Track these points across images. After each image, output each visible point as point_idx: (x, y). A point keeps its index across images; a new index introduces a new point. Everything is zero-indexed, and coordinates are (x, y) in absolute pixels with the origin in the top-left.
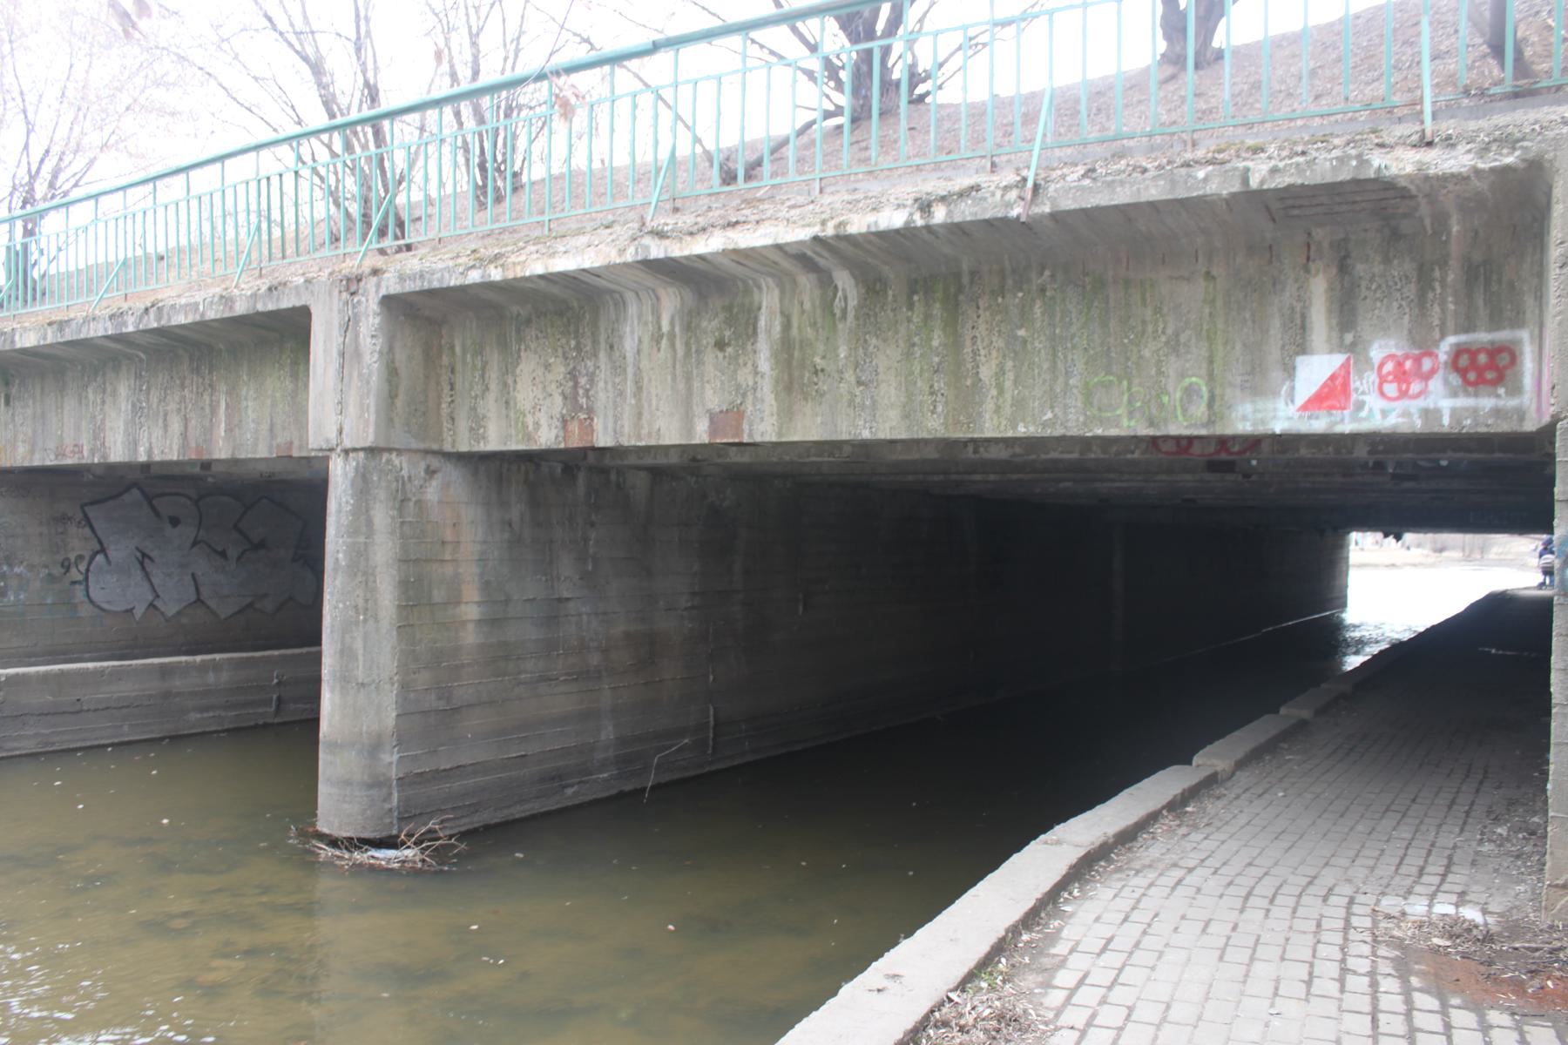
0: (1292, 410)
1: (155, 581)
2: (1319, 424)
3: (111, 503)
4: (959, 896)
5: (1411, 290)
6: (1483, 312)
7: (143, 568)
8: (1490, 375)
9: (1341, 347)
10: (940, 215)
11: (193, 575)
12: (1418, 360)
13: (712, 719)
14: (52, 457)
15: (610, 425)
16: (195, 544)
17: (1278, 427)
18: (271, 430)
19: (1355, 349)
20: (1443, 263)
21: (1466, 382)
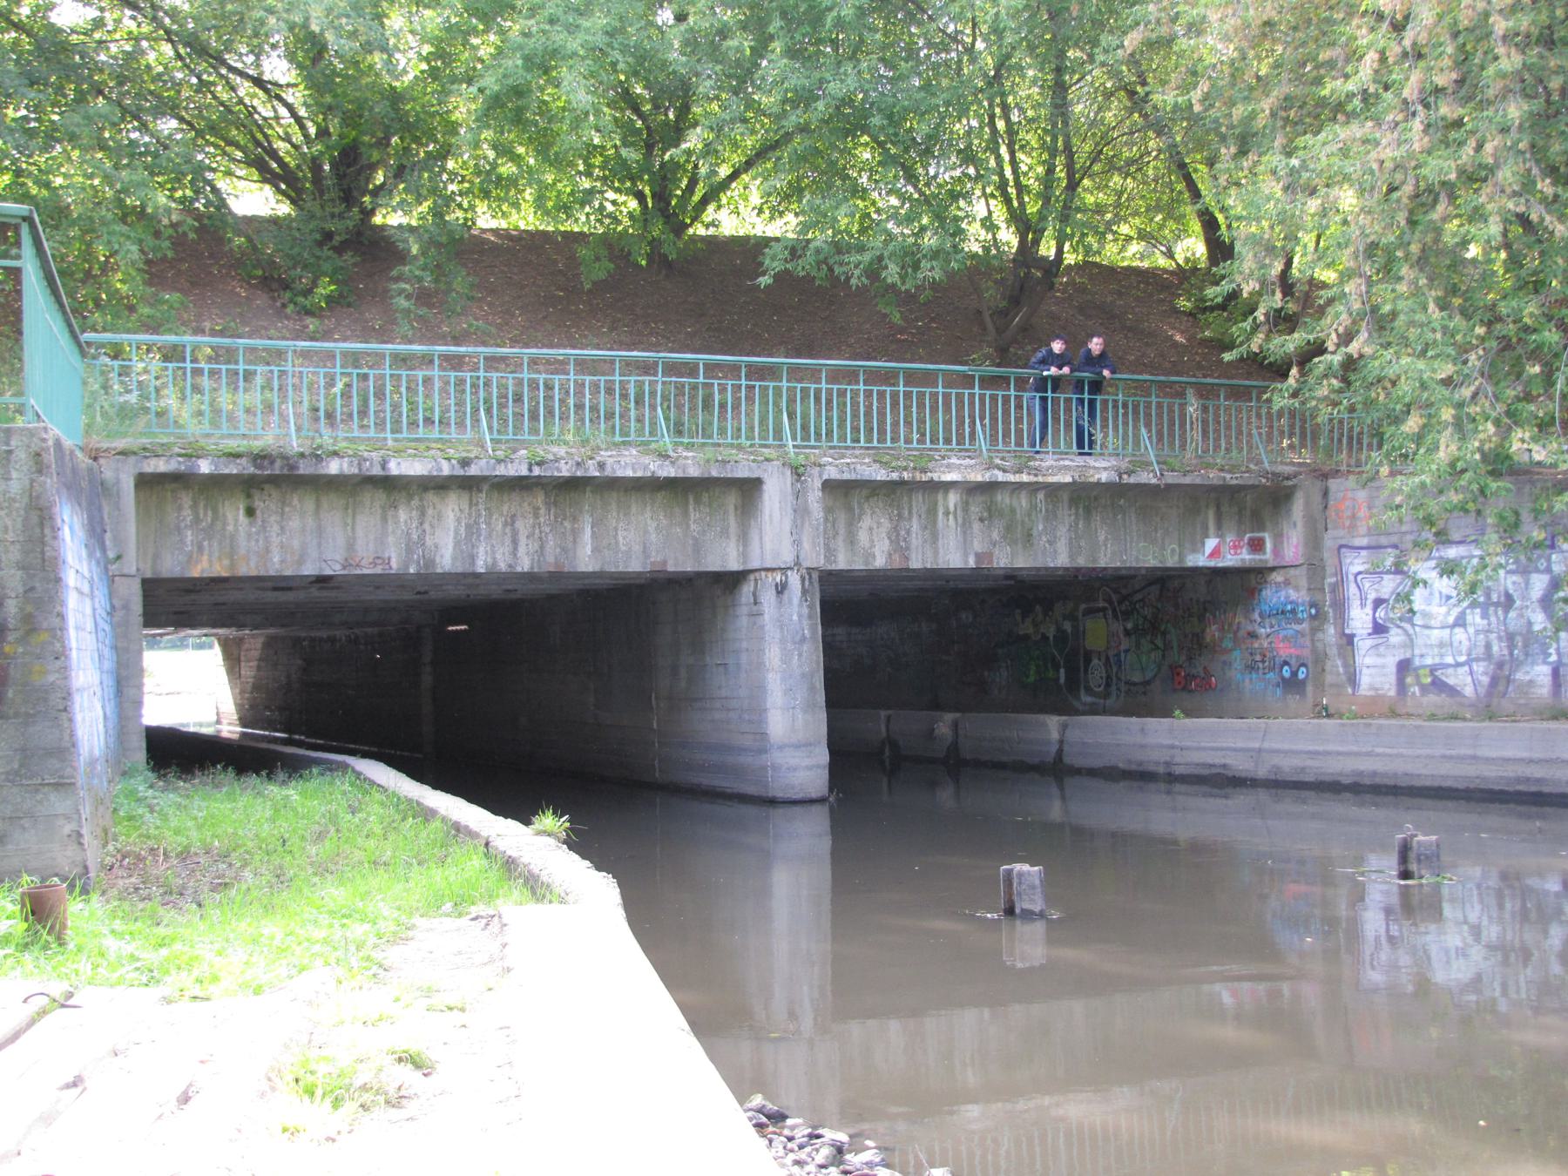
2: (1212, 564)
15: (920, 557)
19: (1221, 536)
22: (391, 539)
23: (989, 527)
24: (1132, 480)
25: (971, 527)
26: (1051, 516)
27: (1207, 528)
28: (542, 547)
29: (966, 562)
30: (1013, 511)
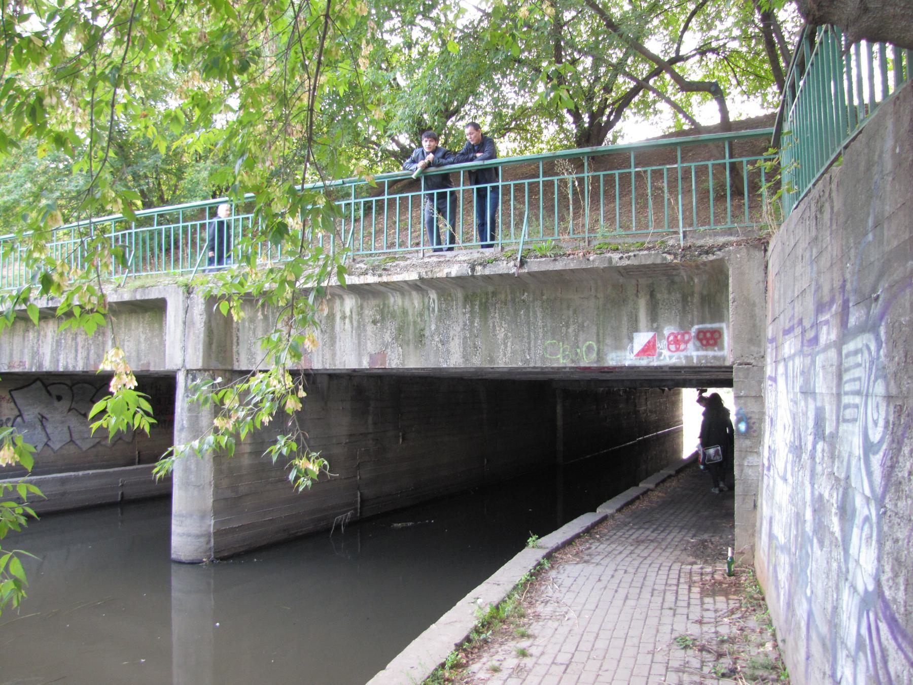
0: (632, 356)
1: (49, 431)
2: (644, 362)
3: (25, 389)
4: (503, 563)
5: (680, 305)
6: (708, 316)
7: (42, 424)
8: (711, 342)
9: (652, 329)
10: (479, 271)
11: (69, 427)
12: (683, 335)
13: (359, 499)
14: (6, 367)
15: (320, 358)
16: (70, 410)
17: (627, 363)
18: (138, 356)
19: (658, 330)
20: (692, 294)
21: (703, 345)
22: (26, 351)
23: (382, 327)
24: (488, 271)
25: (365, 330)
26: (444, 315)
27: (637, 320)
28: (88, 354)
29: (360, 363)
30: (405, 312)
